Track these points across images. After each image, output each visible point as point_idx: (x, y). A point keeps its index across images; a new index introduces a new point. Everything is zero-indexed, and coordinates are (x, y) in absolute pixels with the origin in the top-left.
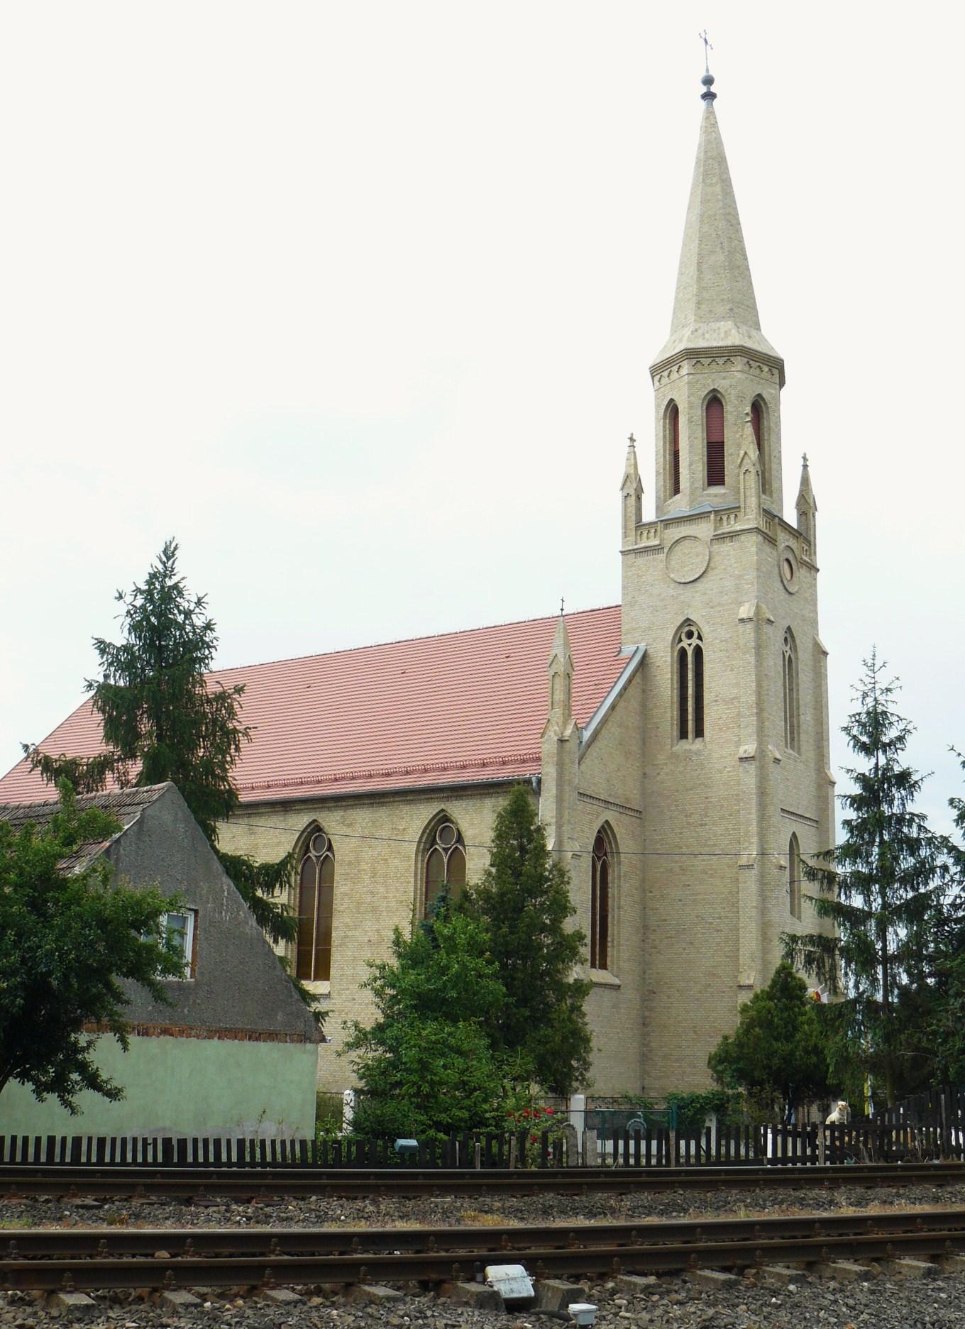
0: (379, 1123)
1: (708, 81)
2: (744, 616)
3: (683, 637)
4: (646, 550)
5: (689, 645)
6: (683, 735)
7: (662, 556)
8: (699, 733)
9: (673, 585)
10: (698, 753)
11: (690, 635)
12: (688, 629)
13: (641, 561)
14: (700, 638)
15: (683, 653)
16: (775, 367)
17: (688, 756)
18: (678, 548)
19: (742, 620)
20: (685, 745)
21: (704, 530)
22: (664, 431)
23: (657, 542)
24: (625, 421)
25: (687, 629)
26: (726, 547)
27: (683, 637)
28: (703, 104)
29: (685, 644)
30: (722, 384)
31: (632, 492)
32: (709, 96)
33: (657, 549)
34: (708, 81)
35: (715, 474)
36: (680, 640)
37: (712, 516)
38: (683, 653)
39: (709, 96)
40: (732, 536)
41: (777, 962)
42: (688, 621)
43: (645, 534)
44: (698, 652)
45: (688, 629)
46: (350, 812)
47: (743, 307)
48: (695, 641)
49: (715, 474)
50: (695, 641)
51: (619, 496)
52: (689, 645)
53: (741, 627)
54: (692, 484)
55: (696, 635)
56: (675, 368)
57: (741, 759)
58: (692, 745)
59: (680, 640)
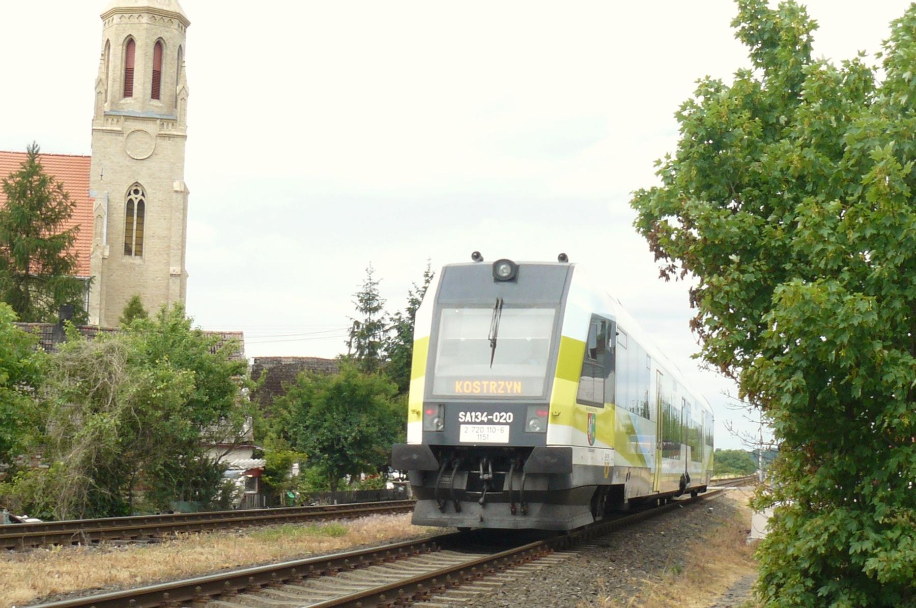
2: (178, 189)
3: (132, 192)
4: (111, 132)
5: (136, 198)
6: (128, 251)
7: (121, 138)
8: (139, 253)
9: (128, 159)
10: (139, 266)
12: (136, 189)
13: (107, 138)
14: (143, 195)
15: (131, 202)
16: (184, 23)
17: (132, 267)
18: (133, 136)
19: (176, 192)
20: (128, 260)
21: (152, 128)
23: (119, 129)
25: (135, 188)
26: (166, 143)
27: (132, 192)
29: (133, 196)
30: (165, 35)
31: (103, 91)
35: (156, 94)
36: (130, 194)
37: (158, 122)
38: (131, 202)
40: (170, 137)
41: (599, 333)
43: (110, 120)
44: (141, 203)
45: (136, 189)
46: (552, 320)
48: (139, 197)
49: (156, 94)
50: (139, 197)
51: (93, 94)
52: (136, 198)
53: (174, 195)
54: (144, 96)
56: (137, 15)
57: (171, 275)
58: (134, 260)
59: (130, 194)
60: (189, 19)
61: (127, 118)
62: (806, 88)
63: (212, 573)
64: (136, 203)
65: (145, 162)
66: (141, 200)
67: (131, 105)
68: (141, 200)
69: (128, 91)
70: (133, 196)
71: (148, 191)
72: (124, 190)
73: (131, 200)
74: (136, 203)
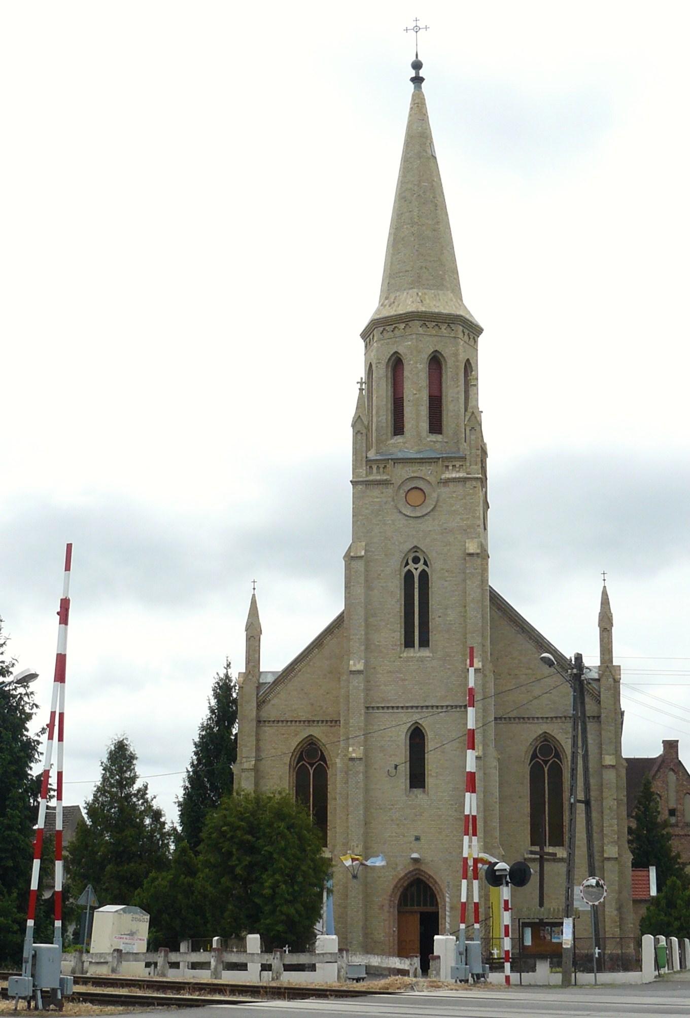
0: (252, 830)
1: (417, 66)
2: (471, 551)
3: (410, 561)
11: (416, 560)
13: (375, 492)
14: (425, 563)
22: (387, 391)
24: (340, 375)
27: (410, 561)
28: (411, 86)
29: (411, 566)
30: (403, 348)
32: (417, 80)
33: (385, 483)
34: (417, 66)
36: (407, 564)
38: (409, 576)
39: (417, 80)
42: (416, 549)
44: (424, 576)
47: (65, 649)
48: (421, 566)
50: (421, 566)
55: (422, 561)
59: (407, 564)
60: (482, 325)
61: (396, 461)
62: (408, 304)
63: (588, 1015)
64: (416, 574)
65: (420, 521)
66: (424, 570)
67: (402, 446)
68: (424, 570)
69: (398, 428)
70: (411, 566)
71: (432, 555)
72: (395, 562)
73: (409, 571)
74: (416, 574)
